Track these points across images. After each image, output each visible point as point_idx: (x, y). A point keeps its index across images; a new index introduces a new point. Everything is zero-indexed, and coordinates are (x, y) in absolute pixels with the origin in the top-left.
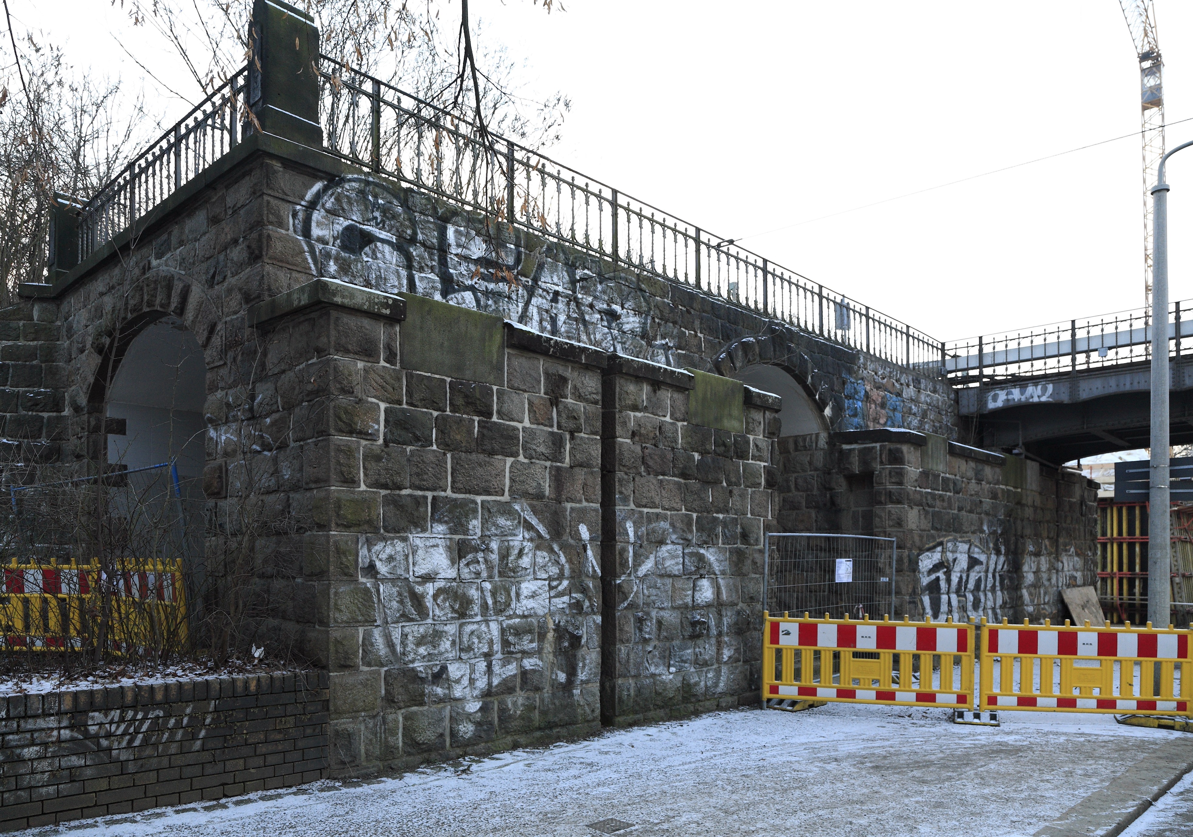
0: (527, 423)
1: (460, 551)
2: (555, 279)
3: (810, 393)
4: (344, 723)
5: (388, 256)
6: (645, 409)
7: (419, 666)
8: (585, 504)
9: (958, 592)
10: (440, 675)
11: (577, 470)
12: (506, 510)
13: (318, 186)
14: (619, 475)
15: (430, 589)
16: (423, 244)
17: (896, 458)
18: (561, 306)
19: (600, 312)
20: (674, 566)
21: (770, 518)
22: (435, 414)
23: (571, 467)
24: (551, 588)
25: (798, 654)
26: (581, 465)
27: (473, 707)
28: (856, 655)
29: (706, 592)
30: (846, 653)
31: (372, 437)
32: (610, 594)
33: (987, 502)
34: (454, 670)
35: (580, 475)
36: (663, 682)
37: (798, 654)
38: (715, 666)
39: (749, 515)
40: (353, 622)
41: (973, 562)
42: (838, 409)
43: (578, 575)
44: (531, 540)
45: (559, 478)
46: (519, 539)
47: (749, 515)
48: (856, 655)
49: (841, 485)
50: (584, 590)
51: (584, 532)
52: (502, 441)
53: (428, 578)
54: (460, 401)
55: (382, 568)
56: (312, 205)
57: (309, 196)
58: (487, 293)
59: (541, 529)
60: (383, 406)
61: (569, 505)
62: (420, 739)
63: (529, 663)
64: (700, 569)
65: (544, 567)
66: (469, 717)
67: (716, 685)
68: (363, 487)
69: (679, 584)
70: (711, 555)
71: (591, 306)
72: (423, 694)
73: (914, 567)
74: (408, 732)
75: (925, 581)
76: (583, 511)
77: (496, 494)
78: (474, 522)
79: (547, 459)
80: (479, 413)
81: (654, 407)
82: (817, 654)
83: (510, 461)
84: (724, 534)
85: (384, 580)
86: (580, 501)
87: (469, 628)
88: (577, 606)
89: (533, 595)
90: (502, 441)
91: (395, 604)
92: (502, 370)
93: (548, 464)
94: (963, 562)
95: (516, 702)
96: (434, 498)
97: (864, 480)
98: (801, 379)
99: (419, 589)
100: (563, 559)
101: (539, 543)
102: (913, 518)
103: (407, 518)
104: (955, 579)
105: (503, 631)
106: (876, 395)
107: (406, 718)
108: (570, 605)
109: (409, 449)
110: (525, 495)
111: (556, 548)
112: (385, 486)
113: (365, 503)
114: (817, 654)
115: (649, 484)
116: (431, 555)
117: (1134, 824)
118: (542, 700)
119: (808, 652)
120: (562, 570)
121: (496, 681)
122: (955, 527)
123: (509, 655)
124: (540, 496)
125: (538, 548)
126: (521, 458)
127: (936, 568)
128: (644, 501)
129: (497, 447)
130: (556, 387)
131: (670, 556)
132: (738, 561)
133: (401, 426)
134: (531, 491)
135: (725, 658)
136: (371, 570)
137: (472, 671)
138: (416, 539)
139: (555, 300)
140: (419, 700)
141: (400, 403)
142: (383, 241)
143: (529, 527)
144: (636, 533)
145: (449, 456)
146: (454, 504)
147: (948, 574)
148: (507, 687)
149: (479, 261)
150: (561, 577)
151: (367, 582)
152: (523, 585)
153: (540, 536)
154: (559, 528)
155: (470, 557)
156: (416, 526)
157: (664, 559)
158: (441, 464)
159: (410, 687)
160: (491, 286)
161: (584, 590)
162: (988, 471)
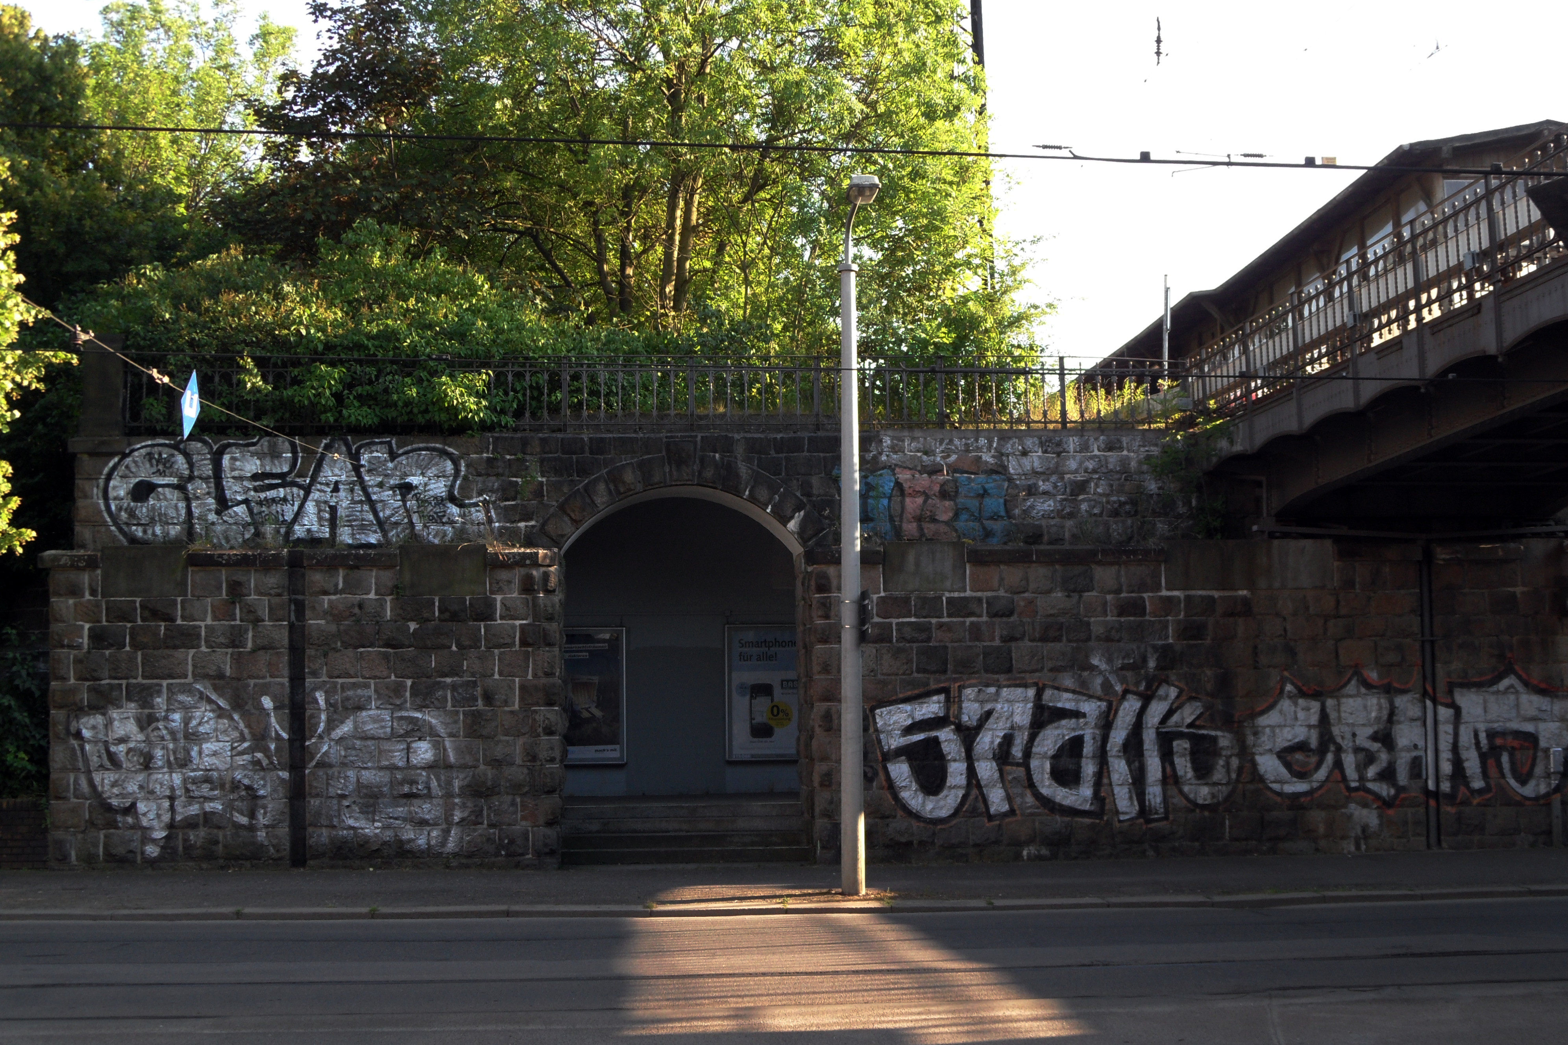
0: (209, 621)
1: (146, 722)
2: (337, 471)
4: (59, 834)
5: (169, 496)
6: (342, 592)
7: (115, 802)
8: (268, 679)
10: (131, 809)
11: (261, 652)
12: (188, 690)
13: (116, 459)
14: (310, 652)
15: (122, 748)
16: (201, 478)
18: (342, 494)
19: (392, 488)
21: (530, 677)
22: (129, 625)
23: (253, 651)
24: (233, 748)
26: (264, 648)
27: (159, 834)
31: (79, 647)
32: (297, 753)
34: (142, 807)
35: (263, 657)
36: (365, 835)
38: (444, 826)
39: (497, 676)
40: (64, 769)
44: (212, 711)
47: (497, 676)
50: (266, 751)
51: (267, 702)
53: (122, 740)
54: (147, 614)
55: (86, 733)
56: (109, 477)
57: (106, 470)
58: (260, 503)
59: (222, 703)
60: (87, 626)
61: (252, 682)
62: (114, 852)
63: (209, 806)
65: (225, 732)
66: (154, 841)
67: (443, 844)
68: (72, 681)
69: (386, 746)
71: (381, 485)
72: (116, 821)
74: (106, 846)
76: (265, 685)
77: (180, 677)
78: (159, 700)
79: (227, 647)
80: (165, 620)
83: (192, 652)
84: (453, 697)
85: (89, 742)
86: (264, 677)
87: (154, 777)
89: (215, 754)
91: (95, 759)
92: (186, 585)
93: (230, 650)
95: (197, 837)
96: (128, 685)
99: (113, 749)
100: (242, 725)
101: (220, 713)
103: (102, 702)
105: (185, 781)
107: (106, 836)
109: (107, 652)
110: (206, 676)
111: (236, 717)
112: (87, 680)
113: (73, 691)
115: (345, 659)
116: (124, 723)
118: (225, 836)
120: (242, 734)
121: (178, 818)
123: (191, 799)
124: (221, 676)
125: (219, 717)
126: (204, 649)
128: (336, 673)
129: (178, 643)
130: (236, 590)
133: (98, 638)
134: (212, 673)
135: (456, 819)
136: (78, 735)
137: (159, 808)
138: (115, 714)
139: (336, 489)
140: (113, 824)
141: (99, 621)
142: (163, 486)
143: (210, 701)
144: (327, 701)
145: (139, 653)
146: (144, 688)
148: (191, 823)
149: (255, 477)
150: (243, 739)
151: (75, 743)
152: (204, 746)
153: (219, 707)
155: (154, 725)
156: (113, 704)
157: (364, 723)
158: (132, 659)
159: (108, 814)
160: (262, 495)
161: (266, 751)
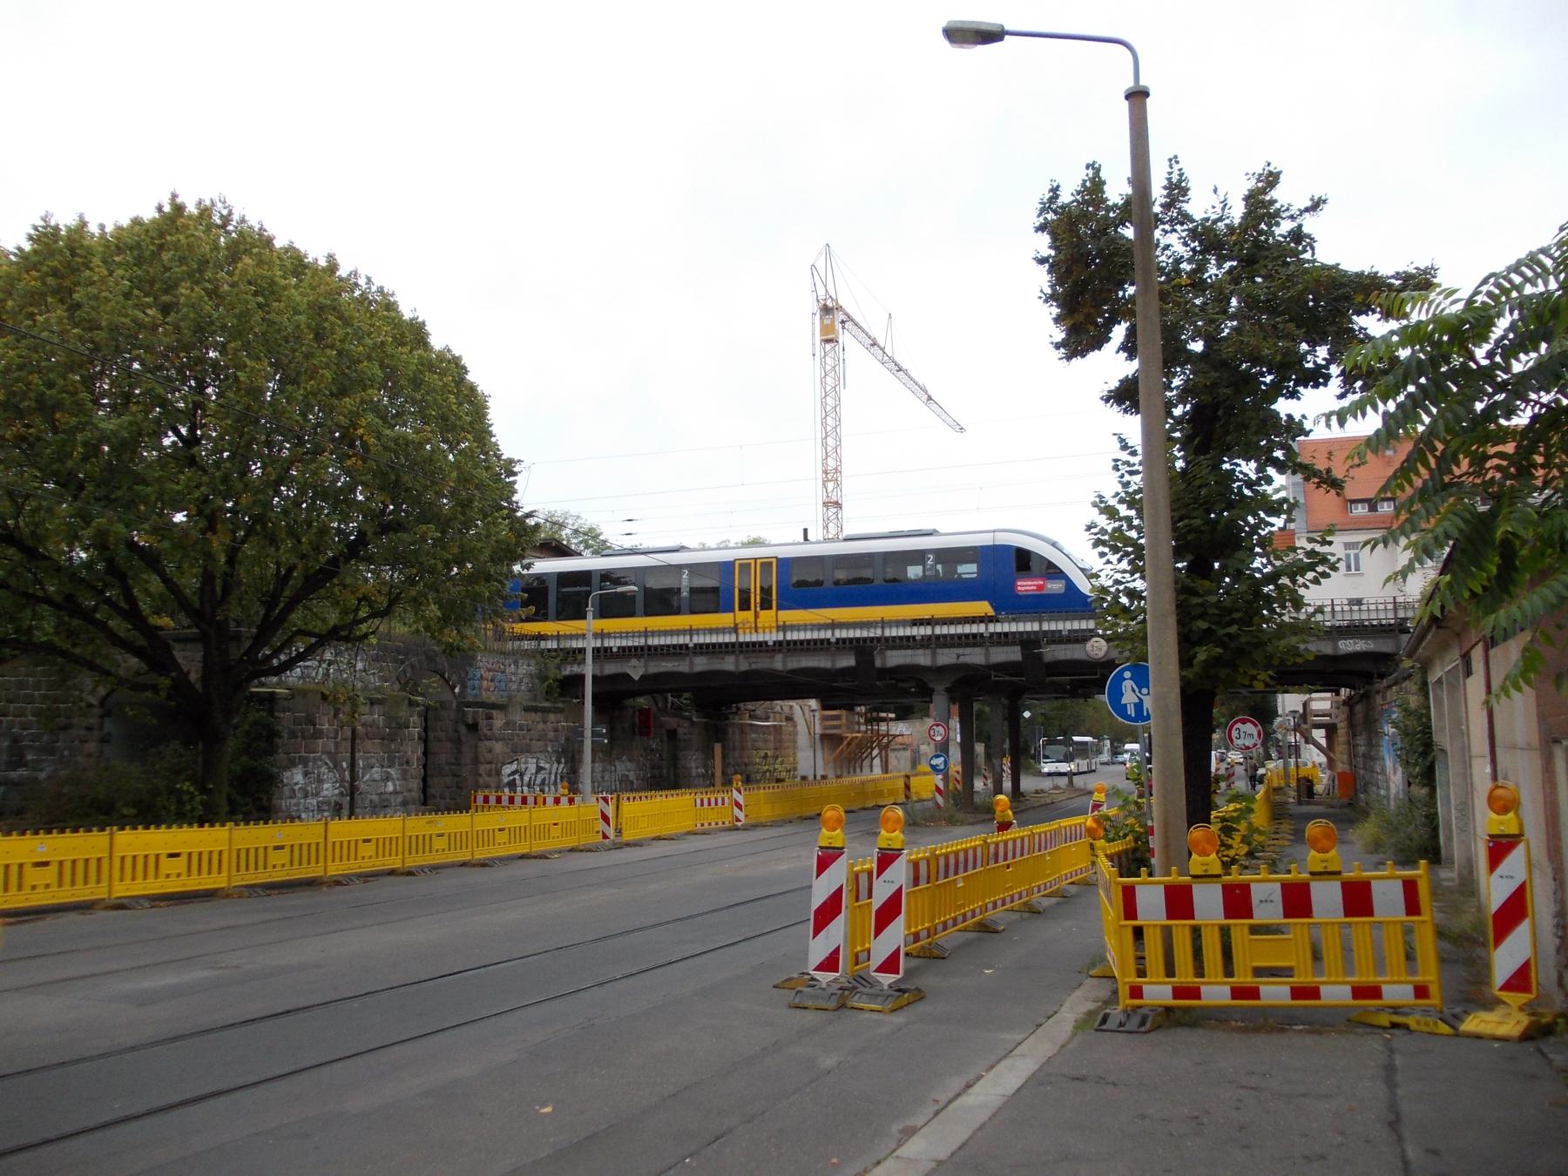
3: (447, 681)
9: (529, 786)
17: (489, 717)
20: (377, 777)
25: (1167, 933)
28: (1254, 930)
29: (390, 787)
30: (1239, 926)
33: (551, 735)
37: (1167, 933)
41: (539, 769)
42: (464, 687)
43: (342, 780)
45: (336, 745)
46: (324, 769)
48: (1254, 930)
49: (463, 729)
52: (318, 734)
64: (388, 778)
70: (392, 771)
73: (499, 773)
75: (506, 780)
81: (371, 714)
82: (1196, 932)
88: (341, 794)
90: (318, 734)
94: (533, 768)
97: (473, 727)
98: (442, 676)
101: (330, 769)
102: (498, 747)
104: (526, 779)
106: (489, 675)
108: (469, 621)
114: (1196, 932)
115: (368, 744)
117: (1017, 1087)
119: (1181, 928)
122: (528, 750)
127: (513, 773)
131: (376, 773)
132: (404, 776)
147: (522, 775)
154: (337, 765)
162: (552, 717)
